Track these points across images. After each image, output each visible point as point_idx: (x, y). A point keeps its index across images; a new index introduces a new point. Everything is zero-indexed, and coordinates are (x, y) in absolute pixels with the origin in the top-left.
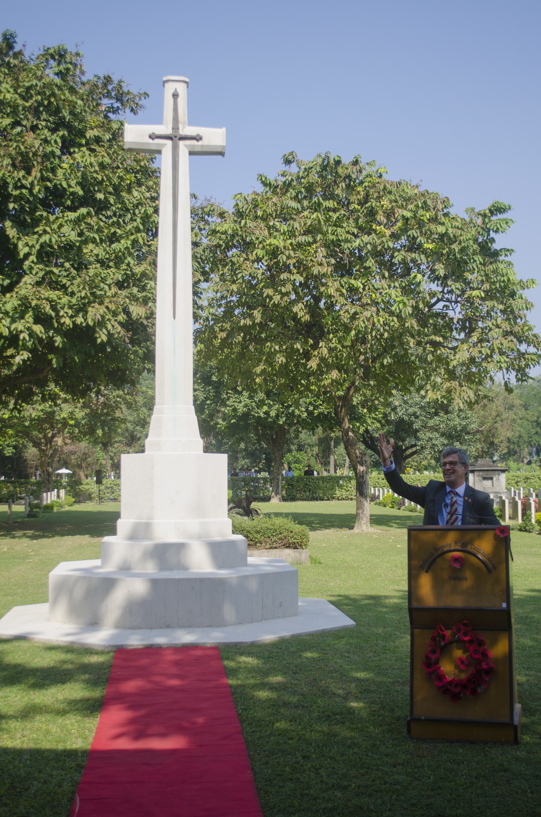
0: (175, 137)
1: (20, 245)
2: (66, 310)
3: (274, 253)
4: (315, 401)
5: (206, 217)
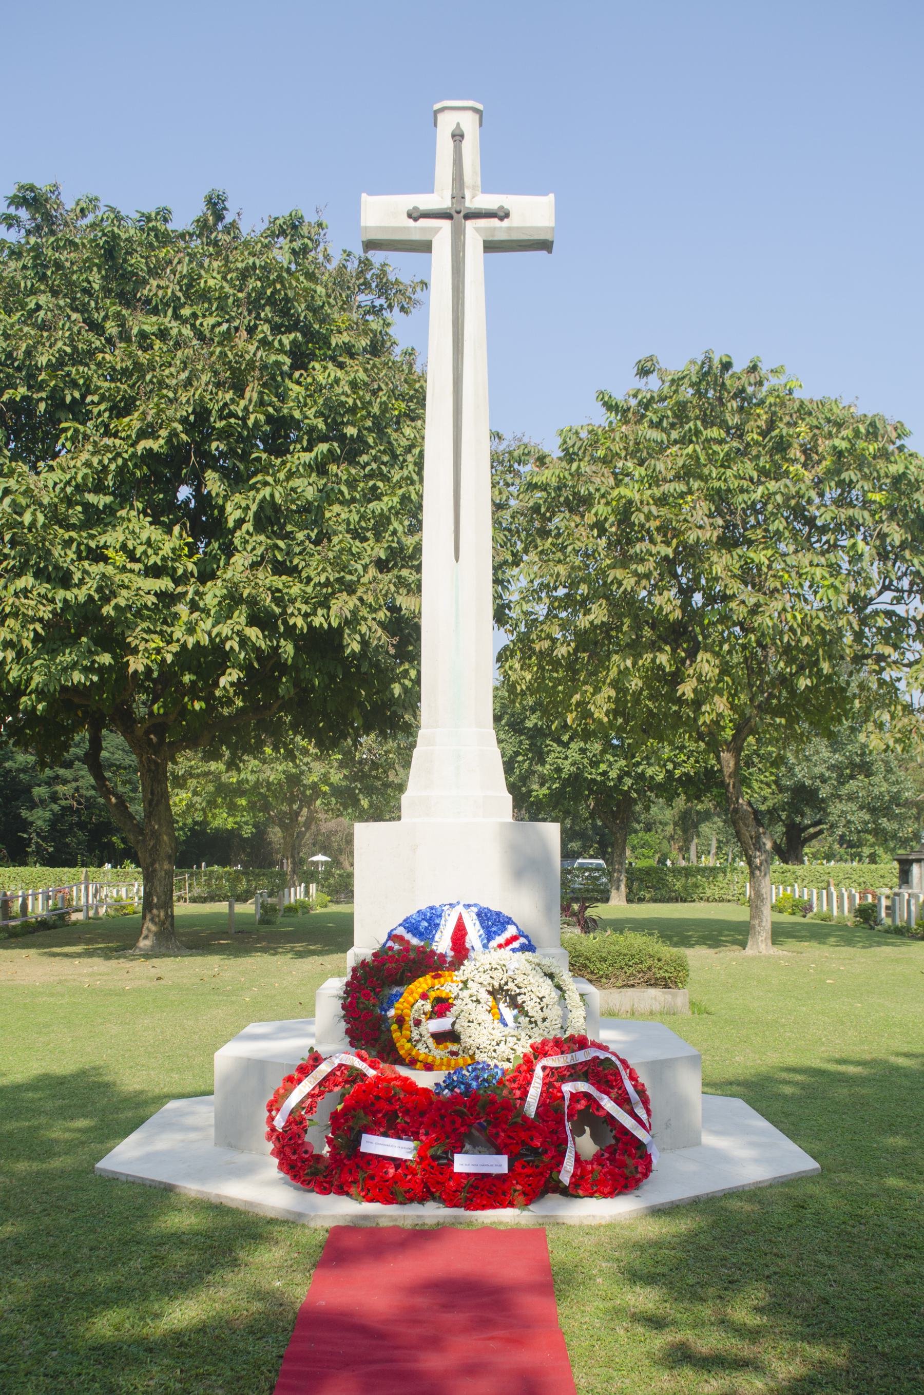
0: (458, 212)
1: (229, 508)
2: (297, 605)
3: (625, 512)
4: (675, 756)
5: (516, 466)
